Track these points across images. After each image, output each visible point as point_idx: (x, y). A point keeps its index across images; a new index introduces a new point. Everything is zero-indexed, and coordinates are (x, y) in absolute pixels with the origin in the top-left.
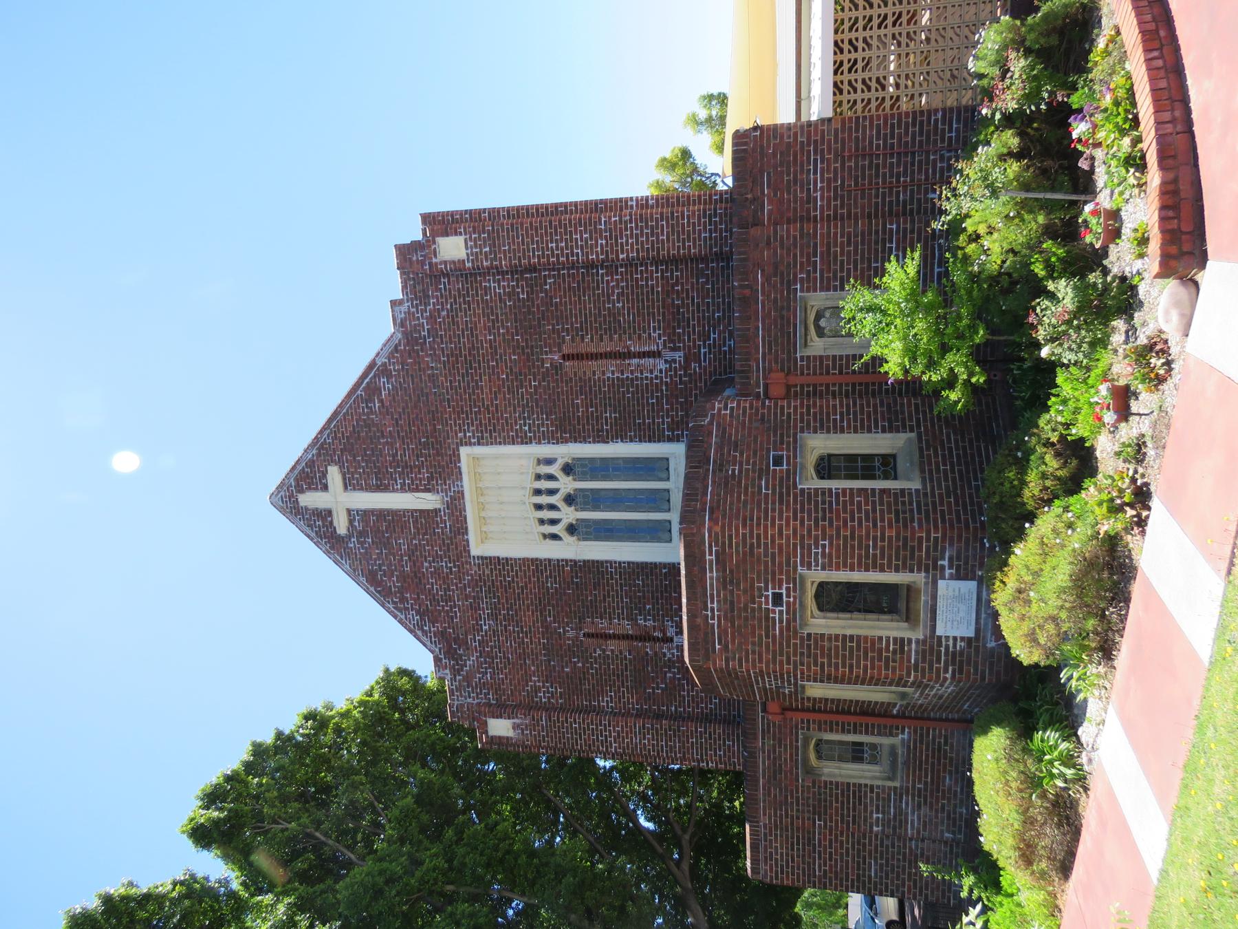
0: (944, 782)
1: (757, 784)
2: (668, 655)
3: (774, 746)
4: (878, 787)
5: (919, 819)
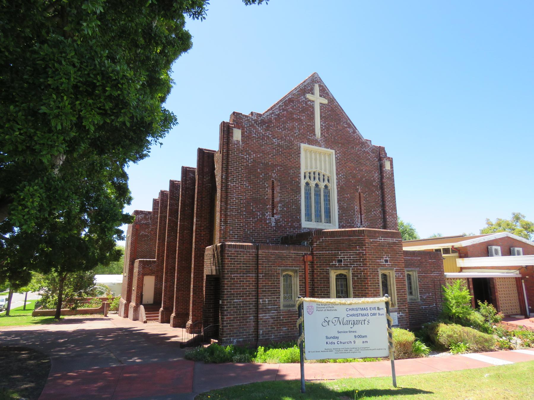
0: (284, 327)
1: (274, 249)
4: (279, 300)
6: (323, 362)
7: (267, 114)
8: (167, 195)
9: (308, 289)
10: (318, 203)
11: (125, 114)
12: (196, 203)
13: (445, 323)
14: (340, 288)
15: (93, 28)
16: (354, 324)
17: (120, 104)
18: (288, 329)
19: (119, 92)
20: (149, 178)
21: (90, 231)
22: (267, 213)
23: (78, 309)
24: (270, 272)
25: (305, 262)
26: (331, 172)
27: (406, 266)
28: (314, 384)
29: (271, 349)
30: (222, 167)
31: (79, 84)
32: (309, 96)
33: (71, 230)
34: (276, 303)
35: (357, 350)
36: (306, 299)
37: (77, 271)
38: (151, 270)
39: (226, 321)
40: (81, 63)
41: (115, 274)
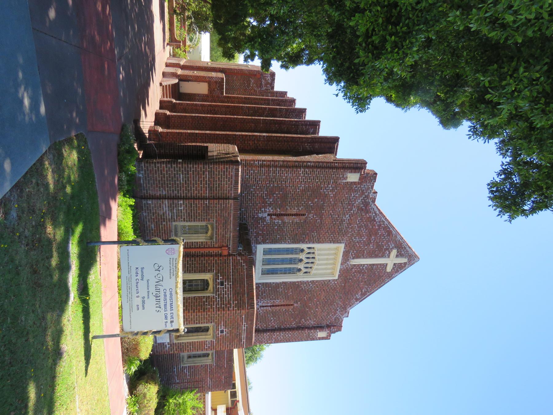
1: (234, 216)
2: (270, 208)
3: (226, 234)
4: (182, 221)
5: (163, 209)
6: (118, 265)
7: (375, 208)
8: (291, 105)
9: (193, 251)
10: (283, 261)
11: (368, 57)
12: (283, 135)
13: (158, 391)
14: (194, 284)
15: (455, 22)
16: (157, 297)
17: (377, 51)
18: (152, 230)
19: (389, 49)
20: (307, 87)
21: (253, 27)
22: (272, 209)
23: (175, 16)
24: (210, 212)
25: (221, 248)
26: (315, 275)
27: (217, 352)
28: (96, 255)
29: (132, 212)
30: (319, 162)
31: (398, 8)
32: (394, 252)
33: (252, 6)
34: (179, 217)
35: (130, 300)
36: (182, 247)
37: (213, 14)
38: (214, 90)
39: (161, 166)
40: (421, 11)
41: (211, 53)
